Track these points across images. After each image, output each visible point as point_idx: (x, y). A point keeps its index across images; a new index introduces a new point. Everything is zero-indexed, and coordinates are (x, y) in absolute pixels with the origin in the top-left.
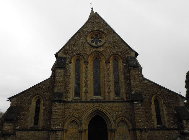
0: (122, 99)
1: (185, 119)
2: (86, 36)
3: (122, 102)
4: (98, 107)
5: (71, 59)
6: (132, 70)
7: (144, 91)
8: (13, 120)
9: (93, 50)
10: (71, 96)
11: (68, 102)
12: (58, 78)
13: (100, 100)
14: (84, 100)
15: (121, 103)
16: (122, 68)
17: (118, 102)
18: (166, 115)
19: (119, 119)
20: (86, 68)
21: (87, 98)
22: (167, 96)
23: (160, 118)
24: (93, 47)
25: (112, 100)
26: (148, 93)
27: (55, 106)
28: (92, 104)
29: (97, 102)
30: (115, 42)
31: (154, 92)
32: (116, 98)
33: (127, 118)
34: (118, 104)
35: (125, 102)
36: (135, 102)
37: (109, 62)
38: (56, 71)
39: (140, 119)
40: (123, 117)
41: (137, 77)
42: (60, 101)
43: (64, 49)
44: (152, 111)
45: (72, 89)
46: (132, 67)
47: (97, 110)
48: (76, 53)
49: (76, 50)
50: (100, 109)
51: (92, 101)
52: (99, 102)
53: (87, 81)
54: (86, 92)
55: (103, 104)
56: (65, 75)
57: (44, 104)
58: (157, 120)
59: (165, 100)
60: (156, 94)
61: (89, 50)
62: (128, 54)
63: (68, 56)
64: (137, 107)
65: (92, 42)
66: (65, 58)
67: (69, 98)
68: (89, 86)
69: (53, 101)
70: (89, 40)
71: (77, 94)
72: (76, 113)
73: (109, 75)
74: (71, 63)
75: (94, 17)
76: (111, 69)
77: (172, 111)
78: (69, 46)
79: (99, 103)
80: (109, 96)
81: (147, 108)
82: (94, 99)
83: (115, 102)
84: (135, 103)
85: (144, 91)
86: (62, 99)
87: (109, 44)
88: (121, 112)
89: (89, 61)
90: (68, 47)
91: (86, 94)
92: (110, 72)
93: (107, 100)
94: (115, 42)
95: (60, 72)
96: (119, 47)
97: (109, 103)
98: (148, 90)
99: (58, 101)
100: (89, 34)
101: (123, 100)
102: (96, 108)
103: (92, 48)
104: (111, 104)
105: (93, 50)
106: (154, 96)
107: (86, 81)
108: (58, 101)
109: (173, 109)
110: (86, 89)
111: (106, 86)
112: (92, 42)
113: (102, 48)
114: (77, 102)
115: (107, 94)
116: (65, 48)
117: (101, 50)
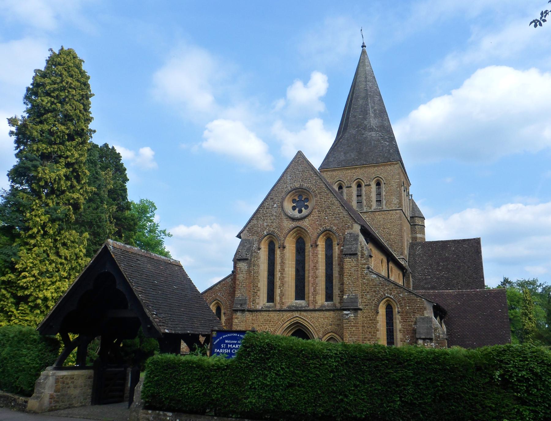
0: (334, 305)
1: (421, 339)
2: (283, 199)
3: (333, 310)
4: (297, 318)
5: (260, 242)
6: (347, 260)
7: (368, 292)
8: (247, 259)
9: (294, 224)
10: (262, 301)
11: (257, 311)
12: (241, 277)
13: (302, 307)
14: (278, 307)
15: (332, 313)
16: (337, 254)
17: (327, 310)
18: (400, 331)
19: (327, 336)
20: (282, 258)
21: (283, 303)
22: (405, 300)
23: (393, 335)
24: (293, 219)
25: (318, 307)
26: (375, 296)
27: (237, 318)
28: (289, 314)
29: (297, 311)
30: (328, 208)
31: (385, 295)
32: (326, 303)
33: (339, 335)
34: (327, 314)
35: (337, 310)
36: (345, 312)
37: (317, 246)
38: (238, 266)
39: (350, 337)
40: (333, 334)
41: (355, 271)
42: (243, 311)
43: (249, 226)
44: (379, 324)
45: (262, 291)
46: (347, 254)
47: (297, 322)
48: (267, 232)
49: (267, 226)
50: (301, 321)
51: (291, 310)
52: (301, 311)
53: (283, 277)
54: (282, 295)
55: (305, 314)
56: (249, 272)
57: (224, 314)
58: (387, 339)
59: (401, 306)
60: (387, 297)
61: (288, 225)
62: (348, 228)
63: (255, 238)
64: (347, 319)
65: (294, 208)
66: (251, 243)
67: (258, 304)
68: (286, 286)
69: (234, 310)
70: (288, 206)
71: (271, 297)
72: (267, 327)
73: (315, 266)
74: (259, 249)
75: (300, 153)
76: (320, 256)
77: (411, 326)
78: (257, 219)
79: (299, 312)
80: (315, 302)
81: (370, 320)
82: (293, 306)
83: (323, 310)
84: (346, 314)
85: (368, 292)
86: (246, 307)
87: (319, 211)
88: (331, 325)
89: (287, 244)
90: (255, 222)
91: (281, 298)
92: (317, 262)
93: (311, 307)
94: (328, 208)
95: (243, 266)
96: (335, 217)
97: (313, 312)
98: (375, 291)
99: (240, 310)
100: (288, 196)
101: (336, 306)
102: (295, 319)
103: (291, 222)
104: (317, 314)
105: (294, 224)
106: (385, 300)
107: (282, 278)
108: (240, 310)
109: (412, 321)
110: (281, 291)
111: (311, 285)
112: (294, 208)
113: (306, 220)
114: (269, 311)
115: (311, 299)
116: (252, 224)
117: (305, 224)
